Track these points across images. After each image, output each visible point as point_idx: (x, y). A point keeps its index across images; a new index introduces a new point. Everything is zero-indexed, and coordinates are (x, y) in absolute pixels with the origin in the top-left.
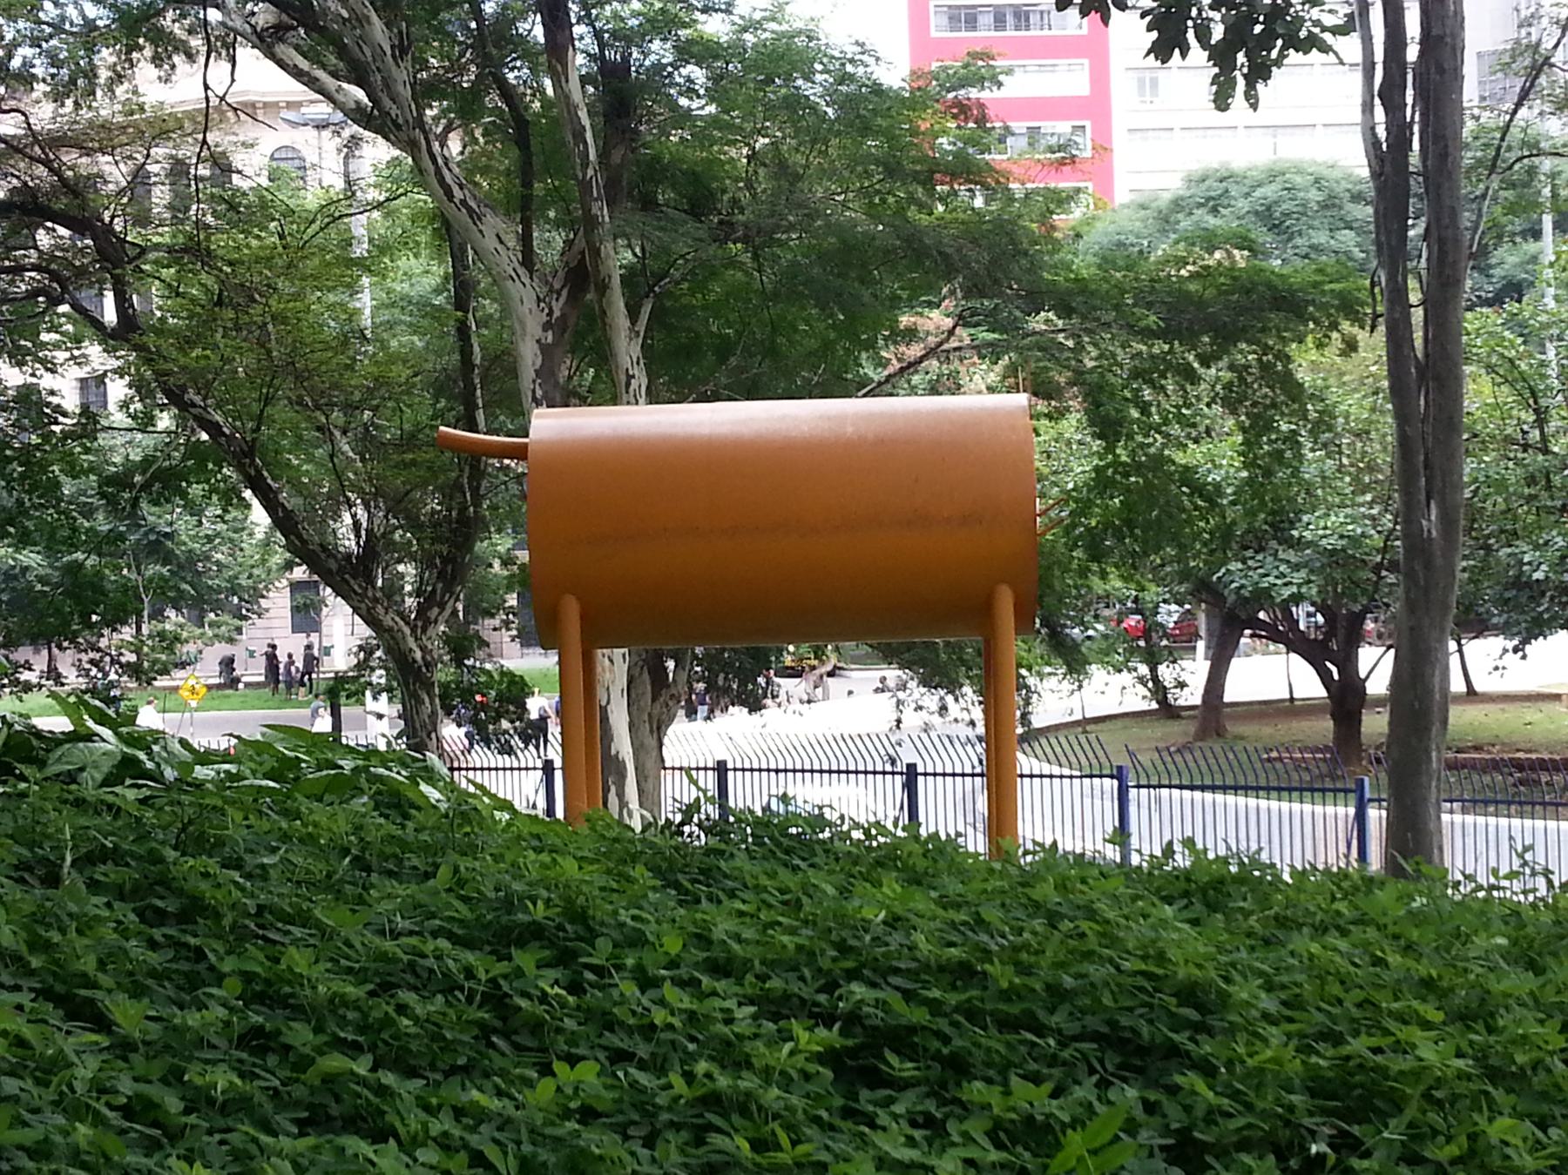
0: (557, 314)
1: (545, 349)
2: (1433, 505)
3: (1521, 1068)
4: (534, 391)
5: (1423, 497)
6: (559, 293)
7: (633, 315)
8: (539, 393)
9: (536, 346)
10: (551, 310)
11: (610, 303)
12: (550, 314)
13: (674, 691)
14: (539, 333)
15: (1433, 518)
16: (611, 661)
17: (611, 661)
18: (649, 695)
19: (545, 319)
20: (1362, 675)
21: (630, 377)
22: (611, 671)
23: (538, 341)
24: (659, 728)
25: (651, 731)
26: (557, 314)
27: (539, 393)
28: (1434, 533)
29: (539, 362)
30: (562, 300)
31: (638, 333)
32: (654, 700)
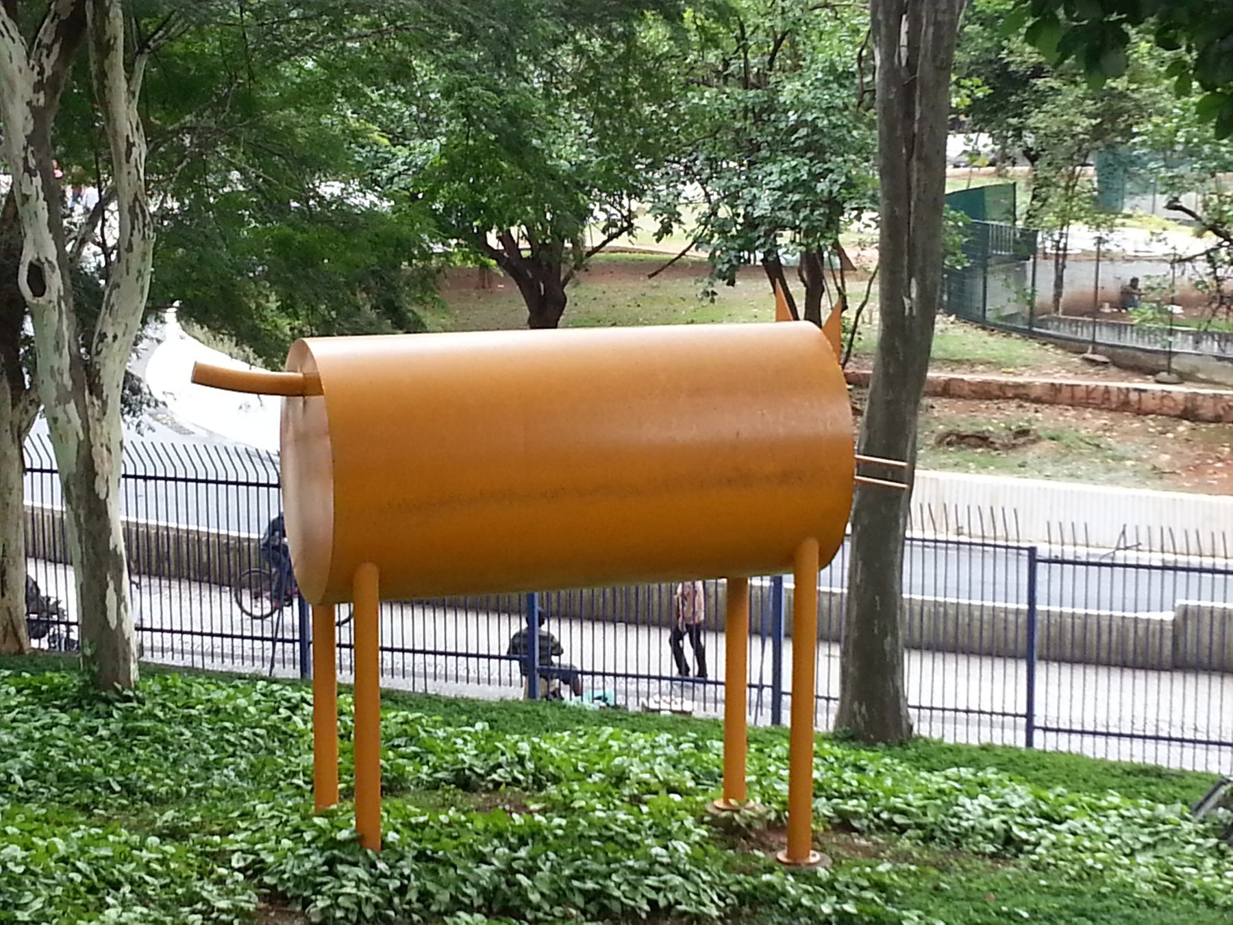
0: (48, 72)
1: (37, 113)
2: (913, 281)
3: (966, 830)
4: (26, 160)
5: (905, 275)
6: (49, 48)
7: (129, 67)
8: (32, 162)
9: (28, 109)
10: (41, 66)
11: (111, 66)
12: (41, 73)
13: (33, 396)
14: (29, 93)
15: (914, 295)
16: (109, 450)
17: (109, 450)
18: (9, 401)
19: (37, 78)
20: (1092, 756)
21: (130, 146)
22: (110, 460)
23: (29, 104)
24: (19, 436)
25: (13, 441)
26: (48, 72)
27: (32, 162)
28: (915, 312)
29: (30, 128)
30: (53, 57)
31: (133, 93)
32: (14, 406)
